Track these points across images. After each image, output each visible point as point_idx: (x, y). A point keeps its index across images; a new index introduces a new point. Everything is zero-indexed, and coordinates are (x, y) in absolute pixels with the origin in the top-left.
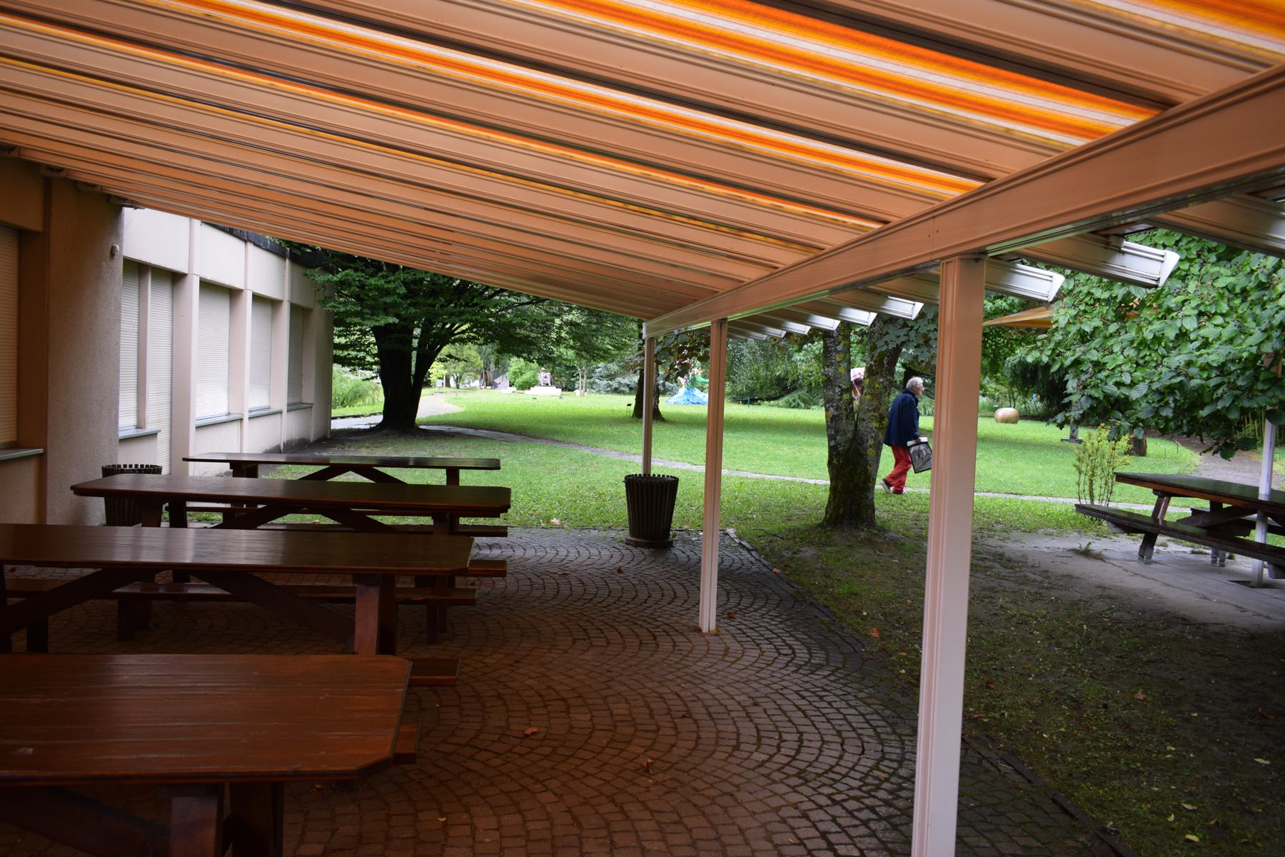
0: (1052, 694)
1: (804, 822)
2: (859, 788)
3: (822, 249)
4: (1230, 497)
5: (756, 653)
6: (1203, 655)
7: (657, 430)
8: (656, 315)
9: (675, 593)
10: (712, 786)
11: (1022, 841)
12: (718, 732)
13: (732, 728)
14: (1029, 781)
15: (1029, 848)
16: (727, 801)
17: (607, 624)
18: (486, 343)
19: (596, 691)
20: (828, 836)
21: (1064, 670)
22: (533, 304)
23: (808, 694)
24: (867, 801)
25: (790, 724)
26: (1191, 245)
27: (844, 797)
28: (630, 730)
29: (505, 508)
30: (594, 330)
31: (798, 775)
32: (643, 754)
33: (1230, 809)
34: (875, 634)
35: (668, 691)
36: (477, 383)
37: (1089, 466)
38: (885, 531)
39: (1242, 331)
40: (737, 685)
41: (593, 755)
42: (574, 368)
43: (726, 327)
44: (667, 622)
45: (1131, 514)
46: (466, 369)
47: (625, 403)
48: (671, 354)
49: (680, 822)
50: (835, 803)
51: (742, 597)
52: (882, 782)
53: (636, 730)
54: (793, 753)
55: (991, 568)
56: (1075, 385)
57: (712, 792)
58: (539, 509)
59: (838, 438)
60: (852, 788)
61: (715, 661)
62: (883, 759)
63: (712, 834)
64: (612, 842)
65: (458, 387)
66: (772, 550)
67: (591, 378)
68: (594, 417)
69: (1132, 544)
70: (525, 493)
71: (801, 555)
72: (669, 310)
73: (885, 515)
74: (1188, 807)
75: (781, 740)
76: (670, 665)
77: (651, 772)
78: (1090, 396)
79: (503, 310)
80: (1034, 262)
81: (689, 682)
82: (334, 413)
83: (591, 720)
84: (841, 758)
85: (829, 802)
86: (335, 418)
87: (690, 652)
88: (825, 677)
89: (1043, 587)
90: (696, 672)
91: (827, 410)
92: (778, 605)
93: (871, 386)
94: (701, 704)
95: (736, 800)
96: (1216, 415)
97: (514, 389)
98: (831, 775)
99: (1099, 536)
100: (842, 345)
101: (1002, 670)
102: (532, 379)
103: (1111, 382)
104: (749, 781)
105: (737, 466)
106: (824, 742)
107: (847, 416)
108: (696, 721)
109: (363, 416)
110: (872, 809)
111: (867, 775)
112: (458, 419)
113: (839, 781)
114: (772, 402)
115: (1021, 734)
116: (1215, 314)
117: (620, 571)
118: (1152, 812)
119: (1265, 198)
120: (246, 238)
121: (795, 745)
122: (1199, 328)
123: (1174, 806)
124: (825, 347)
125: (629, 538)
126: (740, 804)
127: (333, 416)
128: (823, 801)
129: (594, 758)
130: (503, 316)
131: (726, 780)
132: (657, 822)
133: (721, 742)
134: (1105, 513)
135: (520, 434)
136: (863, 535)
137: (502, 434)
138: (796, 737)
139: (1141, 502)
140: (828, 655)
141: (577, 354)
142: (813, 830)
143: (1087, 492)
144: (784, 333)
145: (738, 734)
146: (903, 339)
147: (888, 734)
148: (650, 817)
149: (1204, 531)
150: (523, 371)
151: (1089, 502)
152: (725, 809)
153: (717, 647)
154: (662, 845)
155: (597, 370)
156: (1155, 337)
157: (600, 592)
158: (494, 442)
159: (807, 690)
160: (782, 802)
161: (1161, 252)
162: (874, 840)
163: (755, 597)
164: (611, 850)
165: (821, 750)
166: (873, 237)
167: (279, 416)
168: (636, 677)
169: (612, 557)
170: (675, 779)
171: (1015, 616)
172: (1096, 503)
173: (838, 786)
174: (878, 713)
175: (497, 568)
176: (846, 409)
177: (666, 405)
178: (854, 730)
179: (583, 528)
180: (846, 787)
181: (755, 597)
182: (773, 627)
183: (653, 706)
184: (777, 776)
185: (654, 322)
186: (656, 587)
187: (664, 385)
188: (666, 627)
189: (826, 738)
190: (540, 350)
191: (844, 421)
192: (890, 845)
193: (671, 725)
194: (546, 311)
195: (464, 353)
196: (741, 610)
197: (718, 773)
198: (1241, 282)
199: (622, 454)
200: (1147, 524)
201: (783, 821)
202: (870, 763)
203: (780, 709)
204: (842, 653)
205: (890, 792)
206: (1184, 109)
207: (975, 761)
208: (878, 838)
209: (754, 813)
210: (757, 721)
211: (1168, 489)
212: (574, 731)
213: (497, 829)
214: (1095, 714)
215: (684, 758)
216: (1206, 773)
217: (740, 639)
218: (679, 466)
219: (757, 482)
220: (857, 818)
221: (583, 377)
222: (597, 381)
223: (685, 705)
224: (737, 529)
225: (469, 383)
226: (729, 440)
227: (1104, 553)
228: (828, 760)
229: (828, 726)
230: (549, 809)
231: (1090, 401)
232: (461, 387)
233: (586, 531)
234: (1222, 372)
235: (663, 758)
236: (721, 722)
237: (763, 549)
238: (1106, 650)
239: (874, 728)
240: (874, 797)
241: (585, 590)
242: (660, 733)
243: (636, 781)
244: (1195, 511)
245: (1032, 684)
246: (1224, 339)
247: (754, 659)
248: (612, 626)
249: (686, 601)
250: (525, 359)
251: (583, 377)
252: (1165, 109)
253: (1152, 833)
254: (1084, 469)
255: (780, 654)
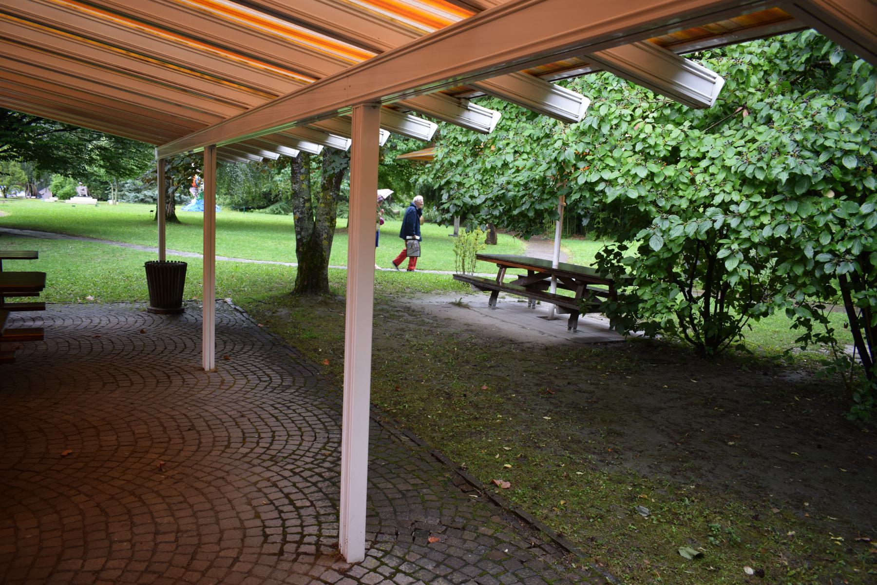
0: (434, 391)
1: (274, 489)
2: (312, 463)
3: (278, 96)
4: (538, 267)
5: (244, 382)
6: (520, 361)
7: (169, 229)
8: (165, 142)
9: (185, 345)
10: (209, 474)
11: (413, 481)
12: (215, 437)
13: (226, 434)
14: (419, 445)
15: (416, 485)
16: (220, 482)
17: (131, 370)
18: (25, 160)
19: (122, 419)
20: (290, 496)
21: (443, 376)
22: (66, 131)
23: (280, 405)
24: (317, 470)
25: (266, 427)
26: (512, 110)
27: (301, 469)
28: (148, 443)
29: (42, 287)
30: (120, 154)
31: (271, 460)
32: (158, 458)
33: (529, 446)
34: (326, 363)
35: (178, 413)
36: (23, 194)
37: (461, 250)
38: (335, 295)
39: (537, 164)
40: (229, 405)
41: (118, 464)
42: (106, 183)
43: (215, 152)
44: (178, 365)
45: (486, 280)
46: (13, 182)
47: (148, 211)
48: (179, 172)
49: (185, 501)
50: (295, 474)
51: (235, 344)
52: (327, 457)
53: (153, 443)
54: (267, 445)
55: (402, 316)
56: (446, 198)
57: (209, 478)
58: (77, 289)
59: (303, 233)
60: (307, 463)
61: (213, 390)
62: (328, 442)
63: (208, 506)
64: (132, 522)
65: (5, 197)
66: (257, 312)
67: (122, 191)
68: (124, 220)
69: (484, 297)
70: (63, 278)
71: (278, 314)
72: (174, 138)
73: (336, 285)
74: (507, 448)
75: (260, 437)
76: (180, 396)
77: (164, 470)
78: (455, 205)
79: (40, 135)
80: (419, 115)
81: (194, 405)
83: (117, 440)
84: (300, 445)
85: (291, 474)
87: (196, 385)
88: (292, 394)
89: (433, 327)
90: (199, 398)
91: (294, 214)
92: (261, 349)
93: (324, 198)
94: (202, 419)
95: (226, 481)
96: (522, 214)
97: (56, 199)
98: (293, 457)
99: (467, 293)
100: (304, 169)
101: (406, 379)
103: (467, 196)
104: (236, 467)
105: (234, 255)
106: (289, 436)
107: (308, 218)
108: (198, 432)
110: (320, 475)
111: (317, 454)
113: (299, 460)
114: (261, 210)
115: (415, 417)
116: (523, 152)
117: (142, 332)
118: (487, 454)
119: (543, 79)
121: (269, 440)
122: (515, 161)
123: (499, 449)
124: (293, 171)
125: (150, 308)
126: (229, 483)
128: (287, 474)
129: (118, 466)
130: (41, 139)
131: (220, 469)
132: (168, 504)
133: (217, 444)
134: (470, 279)
135: (61, 233)
136: (320, 299)
137: (44, 233)
138: (270, 435)
139: (488, 272)
140: (294, 379)
141: (107, 172)
142: (280, 493)
143: (461, 267)
144: (262, 158)
145: (229, 437)
146: (344, 166)
147: (332, 426)
148: (162, 501)
149: (525, 288)
151: (462, 273)
152: (218, 488)
153: (216, 380)
154: (171, 519)
155: (126, 185)
156: (492, 167)
157: (126, 348)
158: (37, 239)
159: (279, 403)
160: (260, 479)
161: (491, 111)
162: (321, 494)
163: (244, 344)
164: (131, 528)
165: (287, 441)
166: (310, 88)
168: (154, 406)
169: (136, 322)
170: (182, 473)
171: (415, 345)
172: (466, 273)
173: (299, 463)
174: (326, 414)
175: (37, 334)
176: (308, 214)
177: (180, 211)
178: (310, 426)
179: (113, 302)
180: (303, 463)
181: (244, 344)
182: (256, 364)
183: (166, 425)
184: (256, 462)
185: (163, 147)
186: (170, 341)
187: (180, 197)
188: (177, 369)
189: (291, 433)
190: (74, 167)
191: (306, 222)
192: (330, 496)
193: (180, 436)
194: (79, 138)
195: (10, 169)
196: (234, 353)
197: (215, 465)
198: (538, 133)
199: (146, 247)
200: (493, 285)
201: (260, 490)
202: (320, 446)
203: (260, 417)
204: (304, 377)
205: (332, 463)
206: (489, 13)
207: (387, 437)
208: (323, 492)
209: (239, 488)
210: (243, 427)
211: (505, 263)
212: (104, 448)
213: (37, 527)
214: (459, 401)
215: (188, 458)
216: (517, 428)
217: (232, 373)
218: (191, 255)
219: (248, 265)
220: (309, 482)
221: (114, 190)
222: (127, 193)
223: (191, 422)
224: (233, 298)
225: (15, 194)
226: (221, 236)
227: (470, 304)
228: (291, 447)
229: (293, 425)
230: (81, 507)
231: (455, 207)
232: (9, 196)
233: (116, 304)
234: (526, 188)
235: (173, 460)
236: (217, 430)
237: (251, 311)
238: (467, 362)
239: (323, 423)
240: (321, 467)
241: (114, 347)
242: (171, 443)
243: (152, 478)
244: (520, 277)
245: (423, 386)
246: (527, 167)
247: (243, 386)
248: (135, 372)
249: (193, 350)
250: (61, 174)
251: (114, 190)
252: (478, 12)
253: (486, 466)
254: (459, 252)
255: (261, 381)
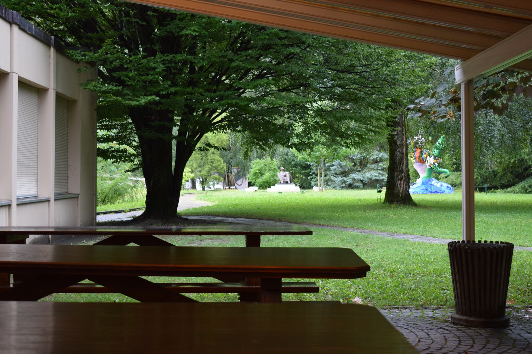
36: (220, 186)
65: (204, 189)
82: (100, 208)
86: (99, 214)
97: (255, 188)
102: (272, 179)
109: (124, 211)
112: (215, 210)
114: (509, 189)
120: (11, 20)
125: (457, 316)
127: (98, 211)
150: (263, 172)
155: (332, 168)
167: (47, 203)
195: (209, 157)
221: (321, 176)
222: (332, 178)
232: (206, 189)
